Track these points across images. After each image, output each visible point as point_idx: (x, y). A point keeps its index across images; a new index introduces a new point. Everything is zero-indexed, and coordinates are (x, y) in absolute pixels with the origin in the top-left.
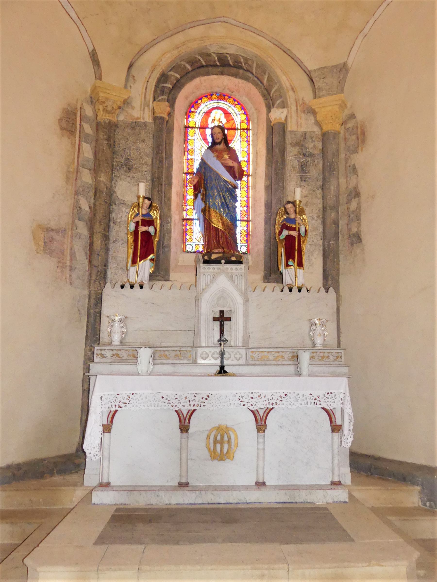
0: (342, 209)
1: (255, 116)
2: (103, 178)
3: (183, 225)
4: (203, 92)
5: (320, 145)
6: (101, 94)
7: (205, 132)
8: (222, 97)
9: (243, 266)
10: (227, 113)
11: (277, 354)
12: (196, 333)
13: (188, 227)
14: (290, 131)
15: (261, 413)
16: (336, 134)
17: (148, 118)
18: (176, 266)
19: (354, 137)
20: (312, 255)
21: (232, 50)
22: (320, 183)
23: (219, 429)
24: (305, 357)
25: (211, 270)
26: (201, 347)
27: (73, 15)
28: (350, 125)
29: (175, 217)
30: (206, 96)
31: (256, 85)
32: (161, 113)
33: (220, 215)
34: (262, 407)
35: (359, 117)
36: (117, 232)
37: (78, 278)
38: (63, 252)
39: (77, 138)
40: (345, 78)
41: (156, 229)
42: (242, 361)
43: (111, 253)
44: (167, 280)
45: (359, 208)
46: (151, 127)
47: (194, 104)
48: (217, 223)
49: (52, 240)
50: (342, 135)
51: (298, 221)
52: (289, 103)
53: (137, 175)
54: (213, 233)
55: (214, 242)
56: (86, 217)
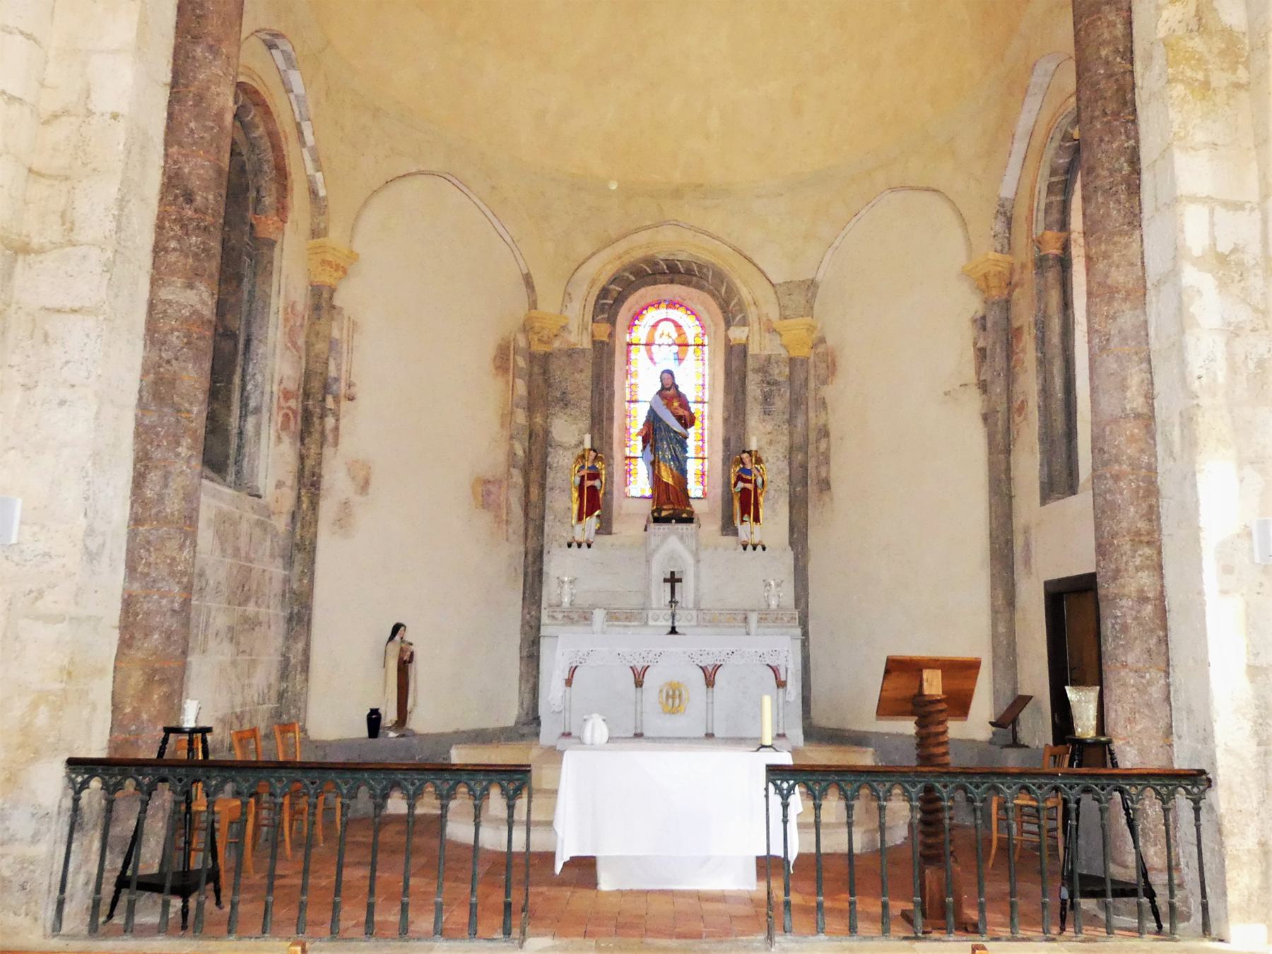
0: (811, 448)
1: (713, 329)
2: (538, 420)
3: (626, 465)
4: (649, 300)
5: (787, 371)
6: (537, 324)
7: (650, 350)
8: (672, 304)
9: (693, 525)
10: (678, 326)
11: (729, 616)
12: (647, 596)
13: (632, 467)
14: (751, 355)
15: (710, 669)
16: (805, 361)
17: (586, 343)
18: (619, 514)
19: (824, 365)
20: (777, 503)
21: (683, 257)
22: (786, 416)
23: (670, 685)
24: (753, 618)
25: (662, 530)
26: (652, 609)
27: (508, 239)
28: (821, 349)
29: (618, 457)
30: (653, 305)
31: (713, 296)
32: (601, 336)
33: (671, 469)
34: (710, 663)
35: (830, 342)
36: (553, 479)
37: (514, 533)
38: (499, 505)
39: (511, 376)
40: (814, 296)
41: (601, 482)
42: (694, 623)
43: (547, 503)
44: (610, 533)
45: (828, 449)
46: (590, 357)
47: (637, 315)
48: (667, 478)
49: (489, 493)
50: (811, 360)
51: (755, 472)
52: (751, 321)
53: (575, 412)
54: (663, 487)
55: (664, 497)
56: (521, 463)
